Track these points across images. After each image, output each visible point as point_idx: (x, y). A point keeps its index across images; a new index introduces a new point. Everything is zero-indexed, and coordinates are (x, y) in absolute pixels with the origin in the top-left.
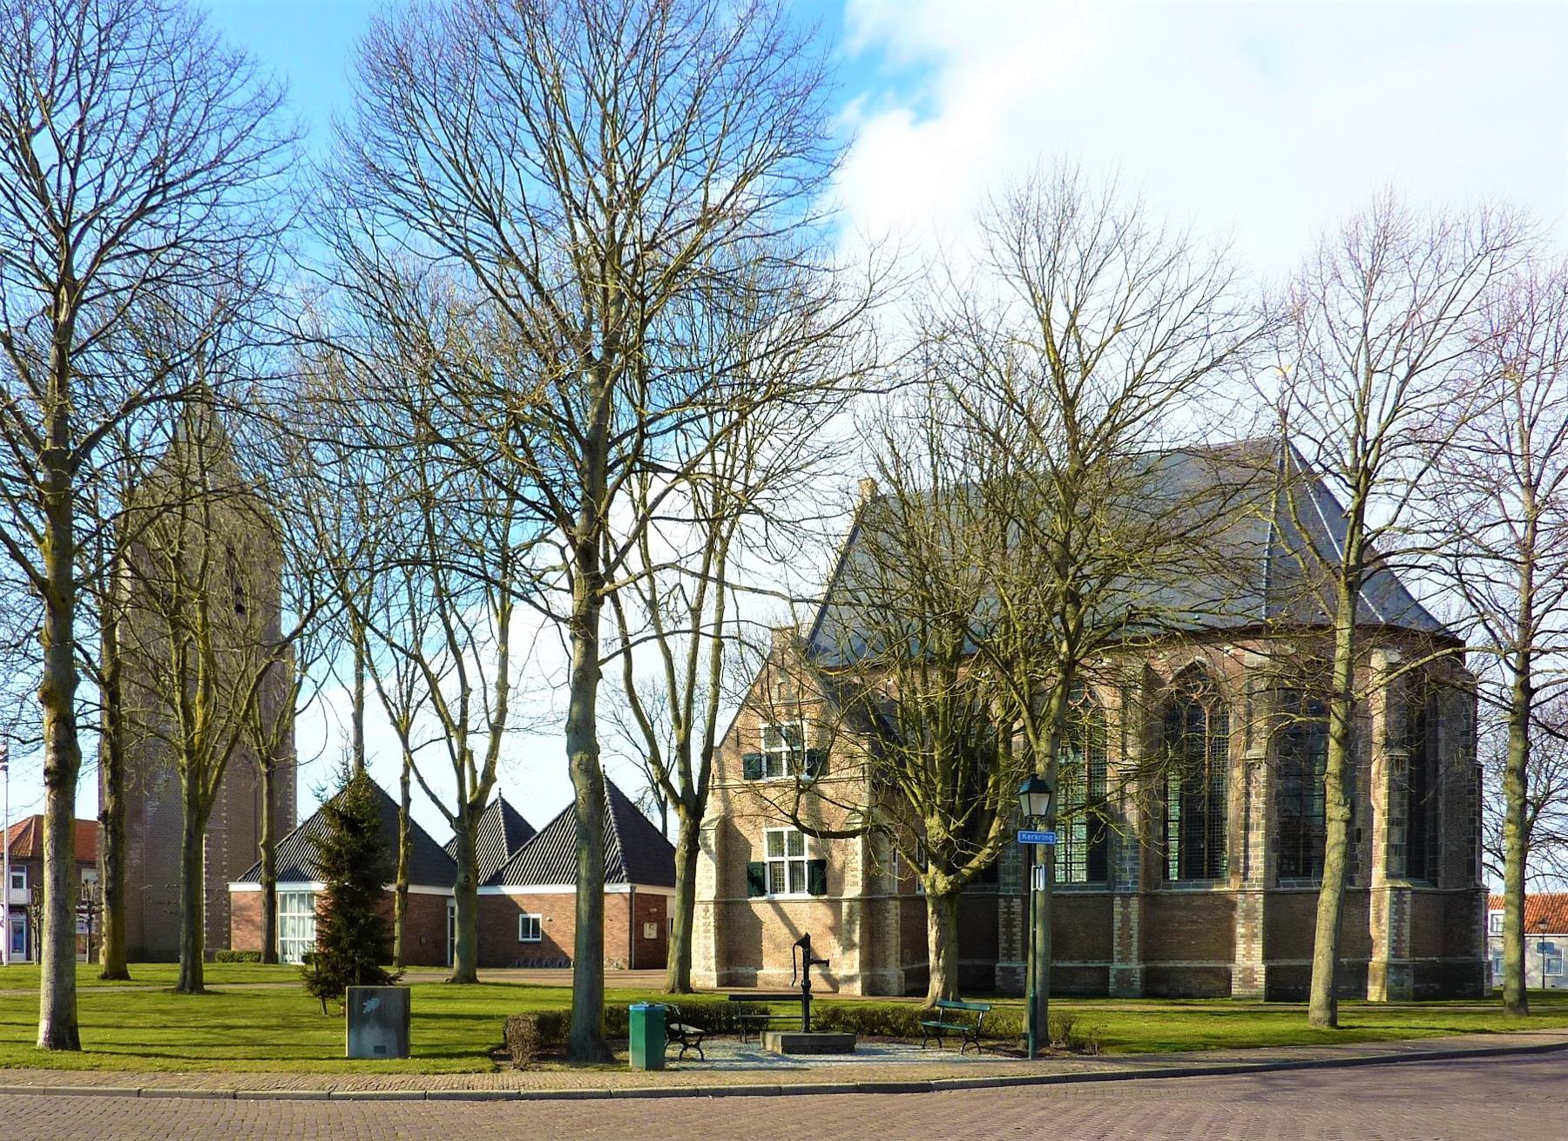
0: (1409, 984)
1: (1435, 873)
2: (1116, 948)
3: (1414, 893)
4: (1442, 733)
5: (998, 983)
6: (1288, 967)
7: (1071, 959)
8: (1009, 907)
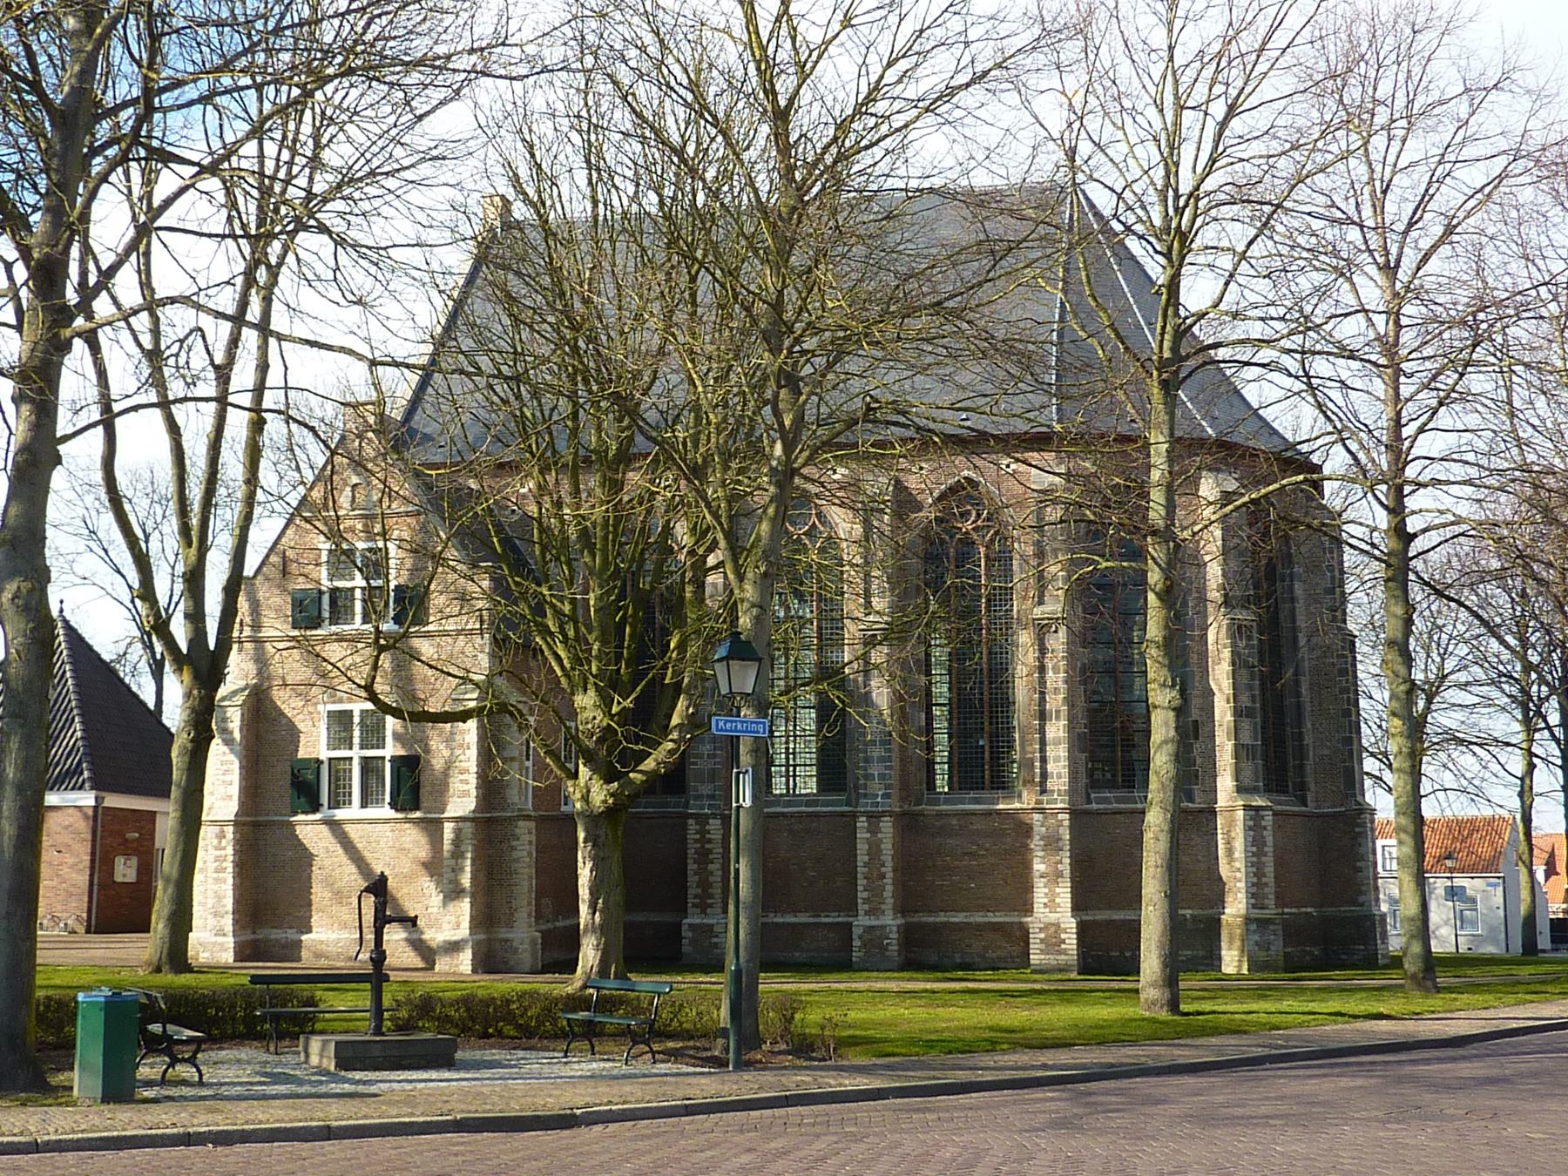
0: (1277, 947)
1: (1302, 787)
2: (862, 895)
3: (1275, 814)
4: (1299, 589)
5: (686, 949)
6: (1110, 922)
7: (795, 911)
8: (703, 832)
